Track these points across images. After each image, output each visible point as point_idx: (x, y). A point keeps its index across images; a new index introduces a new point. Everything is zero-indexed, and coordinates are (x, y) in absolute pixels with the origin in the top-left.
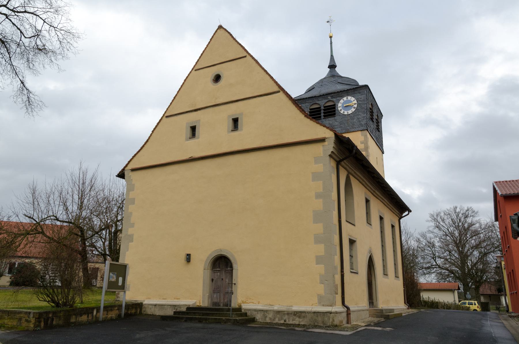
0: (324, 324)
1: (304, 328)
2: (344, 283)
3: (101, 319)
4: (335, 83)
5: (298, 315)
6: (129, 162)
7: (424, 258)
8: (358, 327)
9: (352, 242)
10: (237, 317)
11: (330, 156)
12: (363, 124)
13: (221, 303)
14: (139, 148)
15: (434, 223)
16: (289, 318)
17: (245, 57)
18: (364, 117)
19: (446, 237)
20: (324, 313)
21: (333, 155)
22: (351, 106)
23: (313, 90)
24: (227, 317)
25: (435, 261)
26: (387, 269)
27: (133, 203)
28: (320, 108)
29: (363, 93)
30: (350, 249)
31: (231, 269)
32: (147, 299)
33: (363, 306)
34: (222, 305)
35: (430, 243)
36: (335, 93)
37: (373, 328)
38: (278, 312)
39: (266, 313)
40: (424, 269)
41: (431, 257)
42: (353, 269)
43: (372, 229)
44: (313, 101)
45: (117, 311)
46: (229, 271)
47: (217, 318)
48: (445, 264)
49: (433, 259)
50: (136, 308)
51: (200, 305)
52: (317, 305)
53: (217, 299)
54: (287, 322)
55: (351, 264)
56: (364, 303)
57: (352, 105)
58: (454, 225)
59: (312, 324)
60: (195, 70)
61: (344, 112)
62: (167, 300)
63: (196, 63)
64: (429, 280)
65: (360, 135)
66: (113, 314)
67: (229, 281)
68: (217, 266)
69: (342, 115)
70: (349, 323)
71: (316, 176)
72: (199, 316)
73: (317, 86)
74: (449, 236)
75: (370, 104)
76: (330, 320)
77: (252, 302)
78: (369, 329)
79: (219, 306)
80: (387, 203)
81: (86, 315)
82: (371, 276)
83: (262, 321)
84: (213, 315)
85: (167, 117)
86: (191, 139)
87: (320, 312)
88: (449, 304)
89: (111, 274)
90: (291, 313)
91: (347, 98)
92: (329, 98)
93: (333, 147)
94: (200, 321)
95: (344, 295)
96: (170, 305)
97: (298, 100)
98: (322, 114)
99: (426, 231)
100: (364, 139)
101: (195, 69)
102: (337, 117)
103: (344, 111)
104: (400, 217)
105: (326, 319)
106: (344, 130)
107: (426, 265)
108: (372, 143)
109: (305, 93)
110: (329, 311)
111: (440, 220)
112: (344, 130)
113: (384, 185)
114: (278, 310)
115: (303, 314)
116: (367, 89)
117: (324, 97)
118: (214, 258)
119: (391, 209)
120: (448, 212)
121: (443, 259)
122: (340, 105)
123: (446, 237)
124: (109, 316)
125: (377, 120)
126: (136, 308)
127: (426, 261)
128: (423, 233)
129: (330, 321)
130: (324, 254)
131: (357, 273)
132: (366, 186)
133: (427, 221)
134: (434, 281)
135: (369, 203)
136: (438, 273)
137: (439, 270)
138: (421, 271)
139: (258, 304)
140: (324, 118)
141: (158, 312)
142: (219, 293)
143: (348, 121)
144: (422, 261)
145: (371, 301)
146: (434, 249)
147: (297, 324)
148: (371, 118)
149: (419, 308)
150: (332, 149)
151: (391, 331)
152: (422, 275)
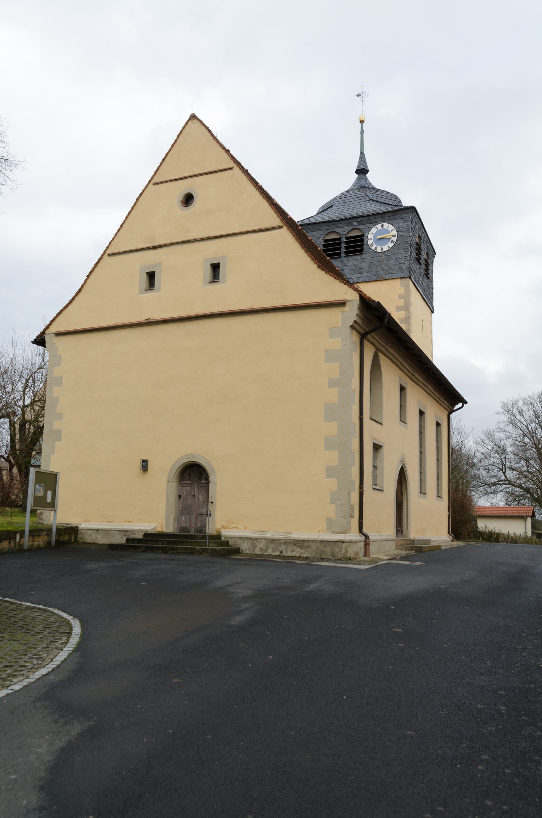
0: (334, 556)
1: (306, 561)
2: (363, 504)
3: (26, 547)
4: (364, 200)
5: (299, 544)
6: (52, 322)
7: (487, 469)
8: (379, 561)
9: (377, 448)
10: (215, 547)
11: (352, 327)
12: (404, 268)
13: (193, 527)
14: (68, 302)
15: (507, 417)
16: (287, 549)
17: (231, 168)
18: (406, 257)
19: (524, 437)
20: (334, 542)
21: (356, 326)
22: (388, 238)
23: (330, 209)
24: (202, 546)
25: (504, 473)
26: (425, 485)
27: (60, 384)
28: (340, 239)
29: (407, 219)
30: (373, 456)
31: (206, 482)
32: (84, 521)
33: (388, 535)
34: (193, 531)
35: (500, 447)
36: (363, 216)
37: (398, 562)
38: (272, 541)
39: (255, 542)
40: (487, 486)
41: (498, 468)
42: (376, 485)
43: (407, 429)
44: (330, 228)
45: (46, 536)
46: (204, 484)
47: (188, 548)
48: (519, 478)
49: (502, 471)
50: (70, 534)
51: (162, 531)
52: (325, 531)
53: (187, 522)
54: (284, 554)
55: (375, 477)
56: (390, 531)
57: (389, 237)
58: (537, 421)
59: (318, 556)
60: (154, 184)
61: (376, 248)
62: (114, 524)
63: (156, 173)
66: (40, 541)
67: (203, 498)
68: (187, 478)
69: (373, 252)
70: (368, 555)
72: (163, 545)
73: (337, 203)
74: (528, 437)
75: (417, 237)
76: (341, 551)
77: (236, 528)
78: (392, 563)
79: (189, 532)
80: (431, 391)
81: (7, 541)
82: (402, 495)
83: (250, 553)
84: (182, 543)
85: (110, 255)
86: (147, 291)
87: (330, 541)
88: (516, 537)
89: (37, 486)
90: (290, 542)
91: (382, 226)
92: (355, 223)
93: (357, 315)
94: (165, 551)
95: (362, 519)
96: (119, 531)
97: (307, 224)
98: (343, 250)
99: (494, 429)
101: (154, 182)
103: (376, 247)
104: (450, 411)
105: (337, 550)
106: (375, 277)
108: (416, 298)
109: (316, 215)
110: (342, 540)
111: (517, 412)
112: (375, 277)
113: (428, 366)
114: (272, 538)
115: (306, 544)
116: (413, 213)
117: (346, 221)
118: (182, 466)
119: (438, 400)
120: (529, 399)
121: (516, 471)
122: (370, 236)
123: (524, 437)
124: (36, 543)
125: (426, 260)
126: (70, 534)
127: (490, 474)
128: (490, 431)
129: (342, 552)
130: (337, 464)
131: (382, 490)
132: (401, 367)
134: (502, 504)
135: (405, 392)
136: (507, 493)
137: (509, 487)
139: (245, 529)
140: (345, 256)
141: (102, 540)
142: (188, 515)
143: (382, 262)
144: (484, 474)
145: (400, 529)
146: (504, 456)
147: (297, 556)
148: (417, 258)
149: (469, 540)
150: (355, 318)
151: (421, 565)
152: (484, 494)
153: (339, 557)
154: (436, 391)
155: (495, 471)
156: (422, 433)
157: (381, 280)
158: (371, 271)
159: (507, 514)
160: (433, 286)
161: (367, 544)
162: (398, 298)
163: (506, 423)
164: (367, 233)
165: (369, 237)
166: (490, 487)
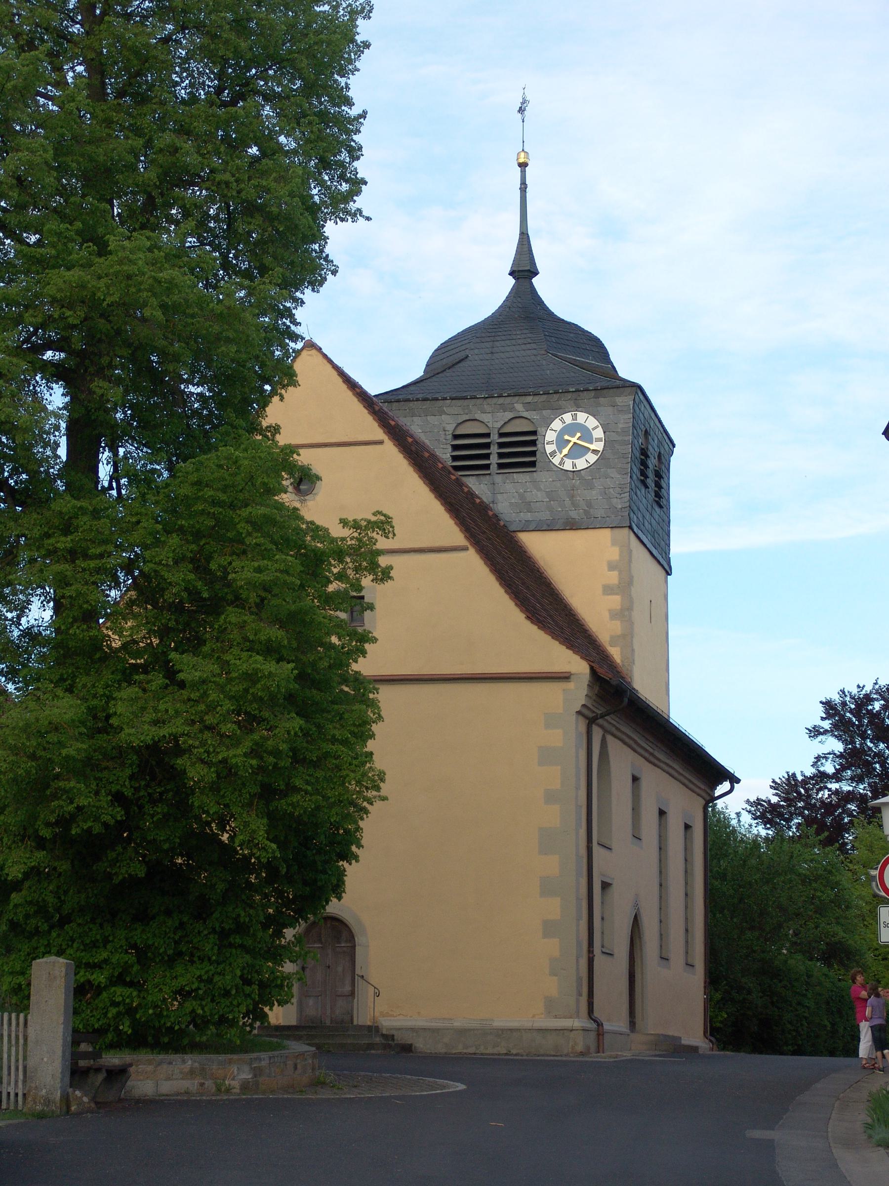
9: (605, 886)
11: (579, 713)
17: (381, 442)
28: (488, 435)
46: (344, 949)
91: (575, 417)
92: (519, 407)
98: (494, 460)
100: (620, 556)
102: (541, 476)
108: (641, 557)
122: (550, 436)
131: (611, 954)
133: (815, 732)
153: (565, 1052)
156: (662, 848)
160: (669, 517)
162: (606, 568)
164: (543, 429)
165: (548, 438)
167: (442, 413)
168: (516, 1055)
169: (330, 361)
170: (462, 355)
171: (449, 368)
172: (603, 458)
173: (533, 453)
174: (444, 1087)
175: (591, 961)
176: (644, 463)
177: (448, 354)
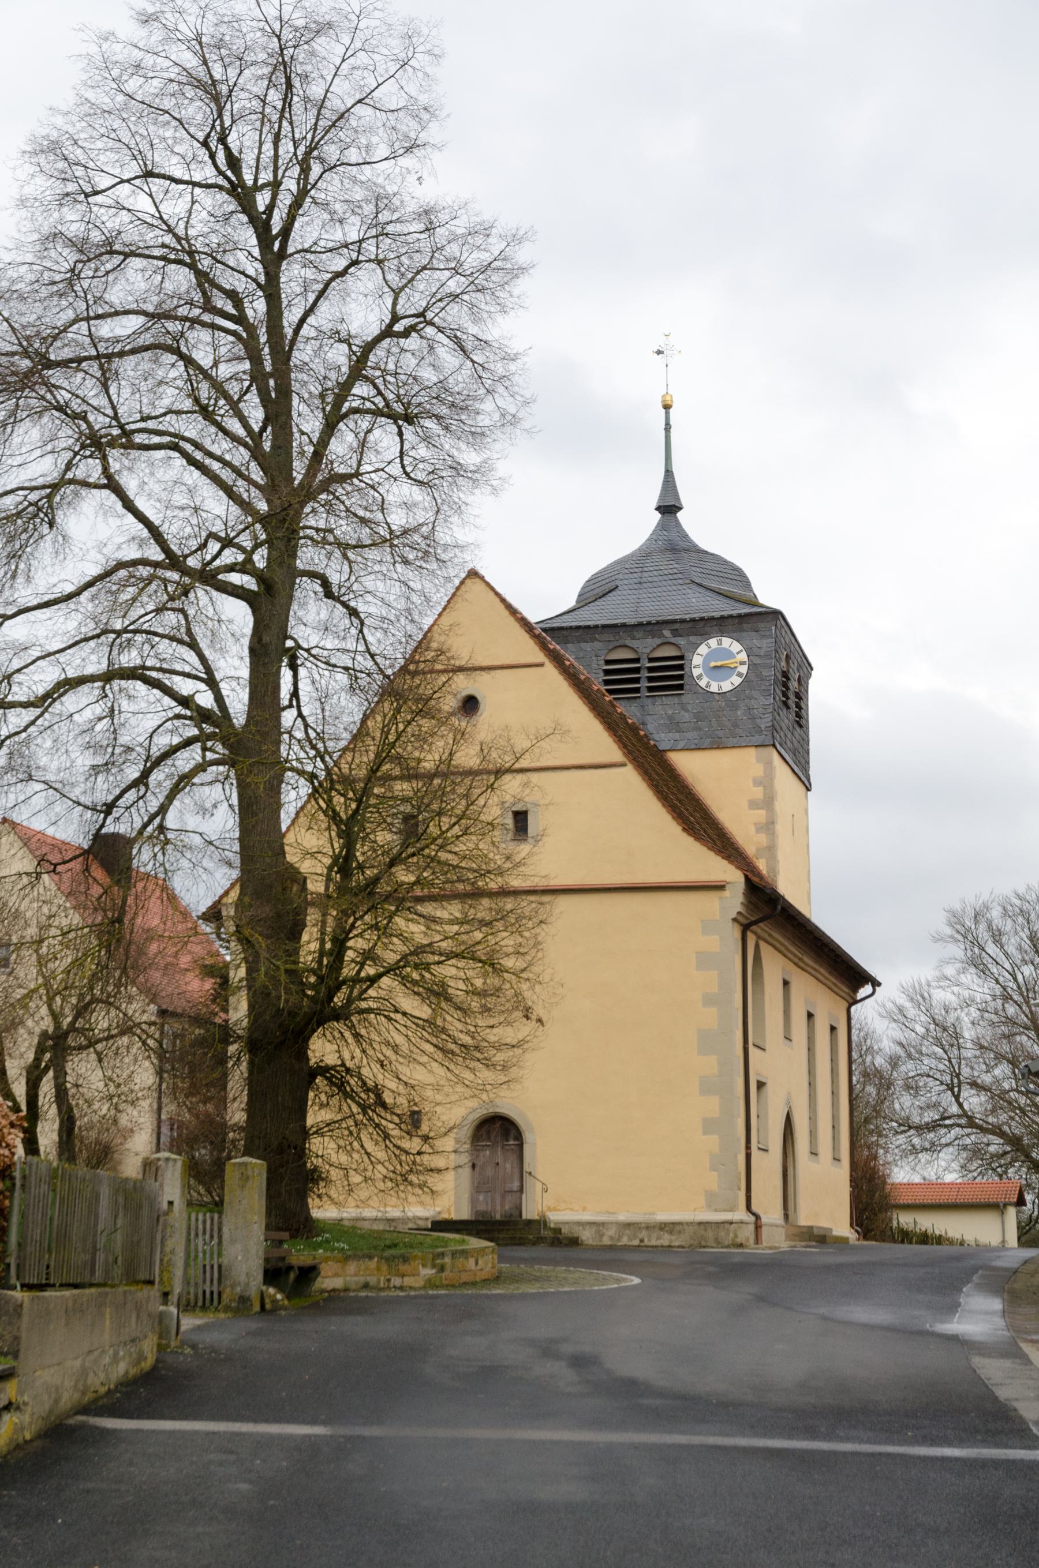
11: (735, 920)
12: (763, 726)
17: (542, 665)
18: (765, 707)
25: (957, 1098)
28: (637, 660)
35: (945, 1029)
38: (628, 1225)
40: (912, 1132)
61: (708, 685)
64: (931, 1174)
65: (754, 760)
68: (484, 1137)
71: (704, 961)
73: (626, 582)
74: (1016, 1002)
91: (720, 643)
92: (667, 633)
98: (644, 684)
102: (687, 698)
105: (722, 1234)
107: (921, 1115)
108: (783, 775)
115: (678, 1228)
117: (649, 628)
120: (1018, 902)
122: (697, 660)
128: (920, 985)
133: (938, 939)
134: (950, 1178)
136: (965, 1148)
138: (901, 1139)
146: (956, 1052)
150: (739, 908)
152: (905, 1154)
153: (726, 1243)
154: (830, 973)
155: (934, 1091)
157: (718, 748)
158: (700, 729)
159: (960, 1200)
160: (808, 736)
161: (758, 1227)
162: (751, 784)
163: (959, 965)
164: (690, 654)
166: (920, 1135)
167: (595, 639)
168: (679, 1247)
169: (492, 589)
170: (612, 585)
171: (600, 598)
172: (747, 680)
173: (681, 677)
174: (618, 1281)
175: (748, 1157)
176: (785, 685)
177: (598, 585)
